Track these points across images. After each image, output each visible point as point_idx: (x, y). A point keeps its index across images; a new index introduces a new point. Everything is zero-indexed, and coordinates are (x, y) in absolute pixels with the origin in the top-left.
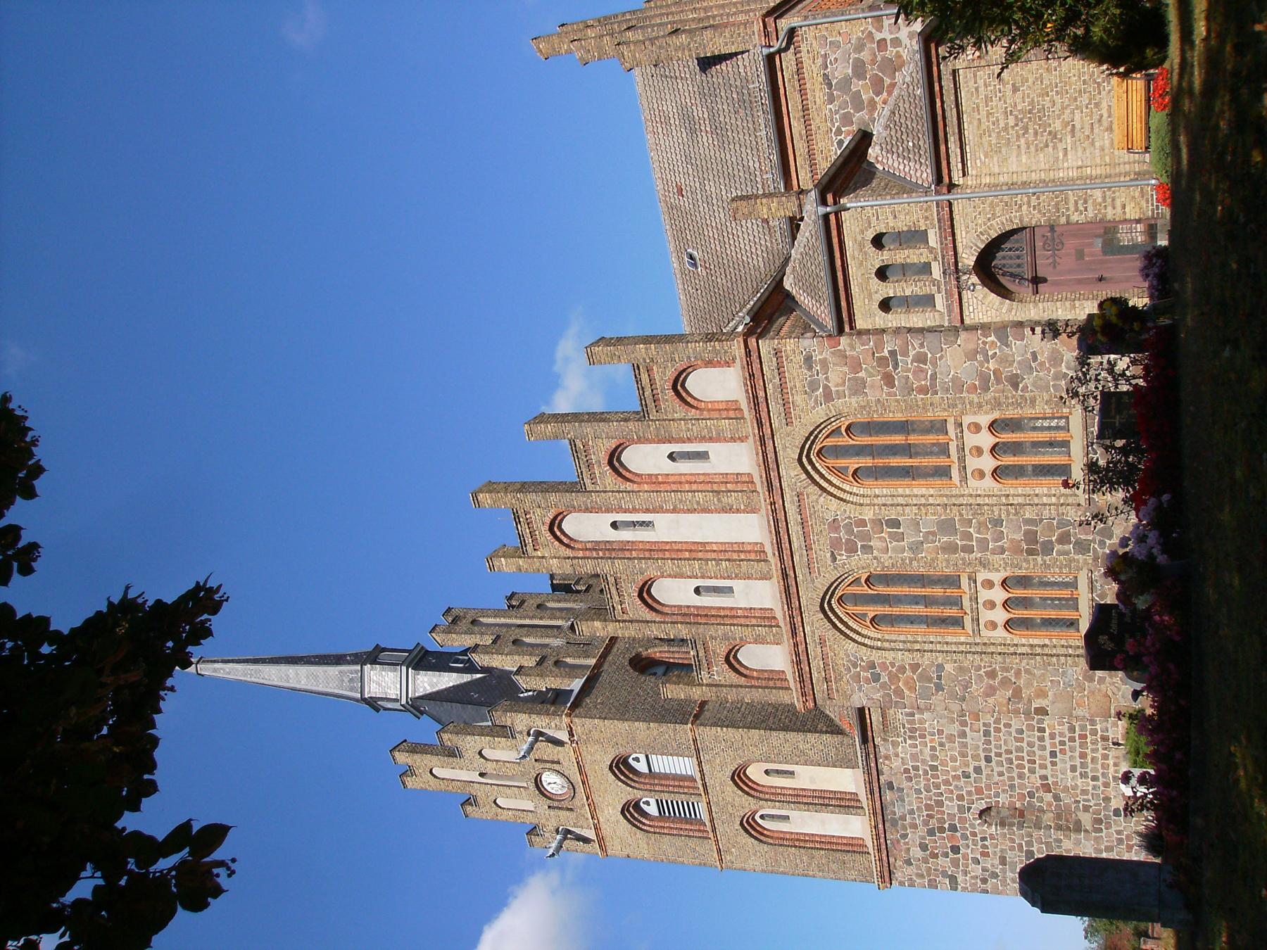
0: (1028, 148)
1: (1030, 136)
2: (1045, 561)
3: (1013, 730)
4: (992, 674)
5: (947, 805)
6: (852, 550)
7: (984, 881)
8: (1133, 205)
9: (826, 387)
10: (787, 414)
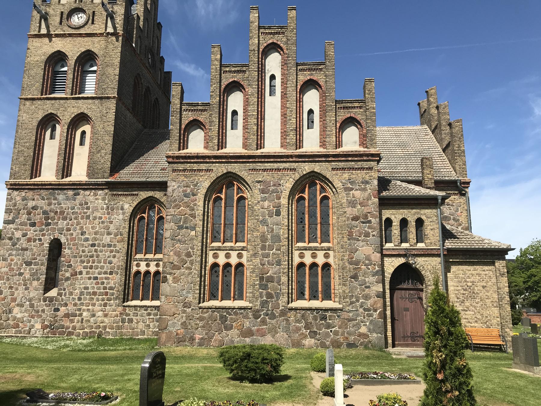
0: (457, 291)
1: (462, 292)
2: (256, 285)
3: (111, 259)
4: (189, 255)
5: (63, 222)
9: (352, 189)
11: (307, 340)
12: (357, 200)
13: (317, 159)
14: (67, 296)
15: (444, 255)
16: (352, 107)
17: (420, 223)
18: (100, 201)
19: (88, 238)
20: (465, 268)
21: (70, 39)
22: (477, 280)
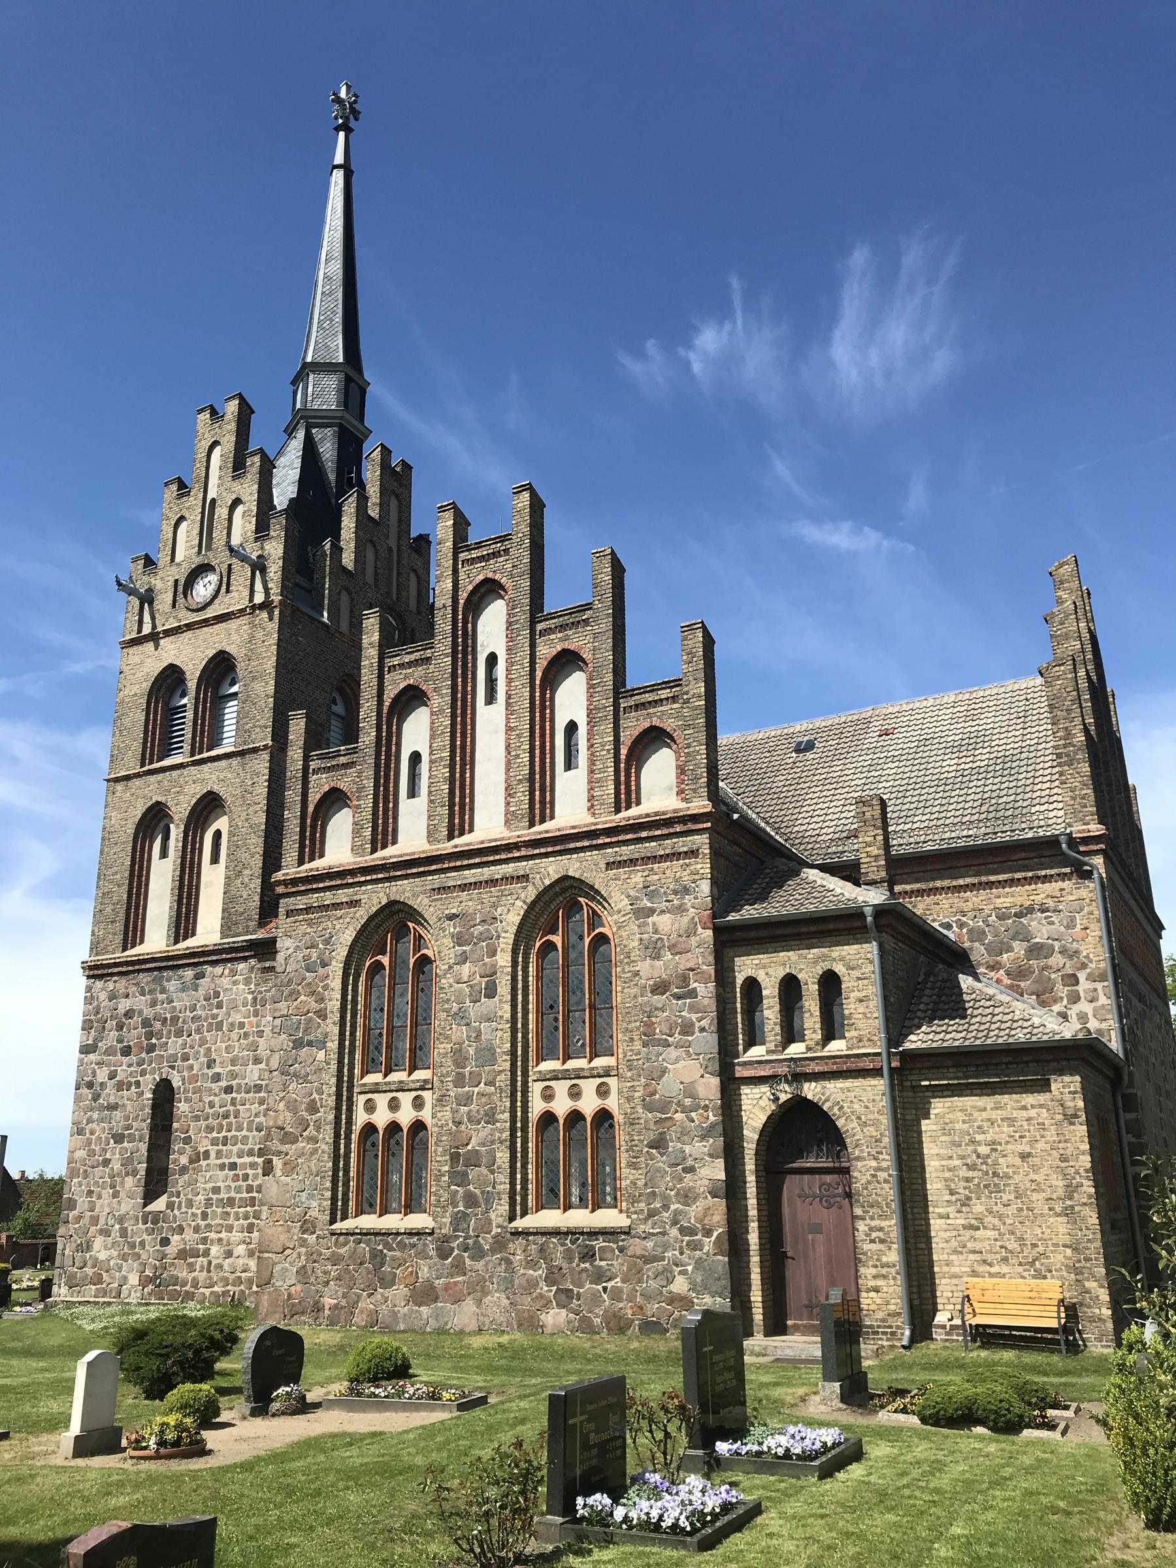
0: (950, 1170)
1: (964, 1172)
4: (313, 1108)
6: (459, 940)
7: (90, 1085)
8: (878, 1301)
9: (652, 911)
10: (620, 864)
11: (552, 1312)
12: (662, 939)
13: (572, 846)
14: (184, 1210)
15: (891, 1070)
16: (656, 701)
17: (830, 984)
18: (242, 987)
19: (219, 1074)
20: (970, 1103)
21: (189, 634)
22: (1004, 1138)
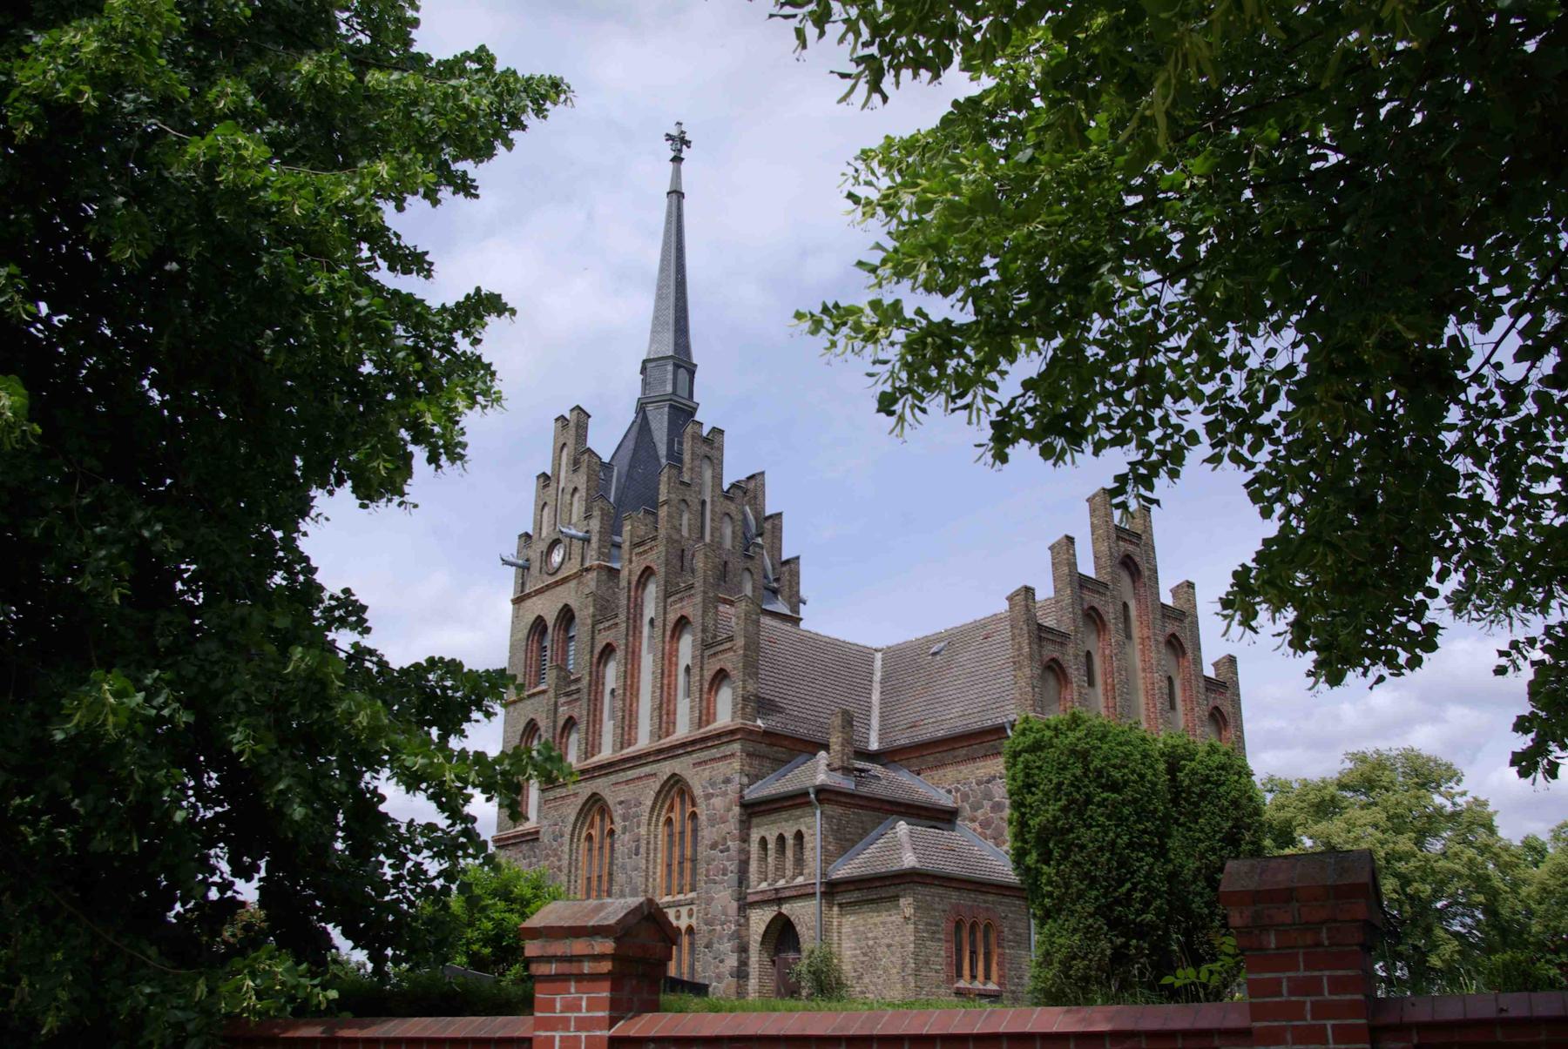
10: (700, 764)
17: (799, 836)
